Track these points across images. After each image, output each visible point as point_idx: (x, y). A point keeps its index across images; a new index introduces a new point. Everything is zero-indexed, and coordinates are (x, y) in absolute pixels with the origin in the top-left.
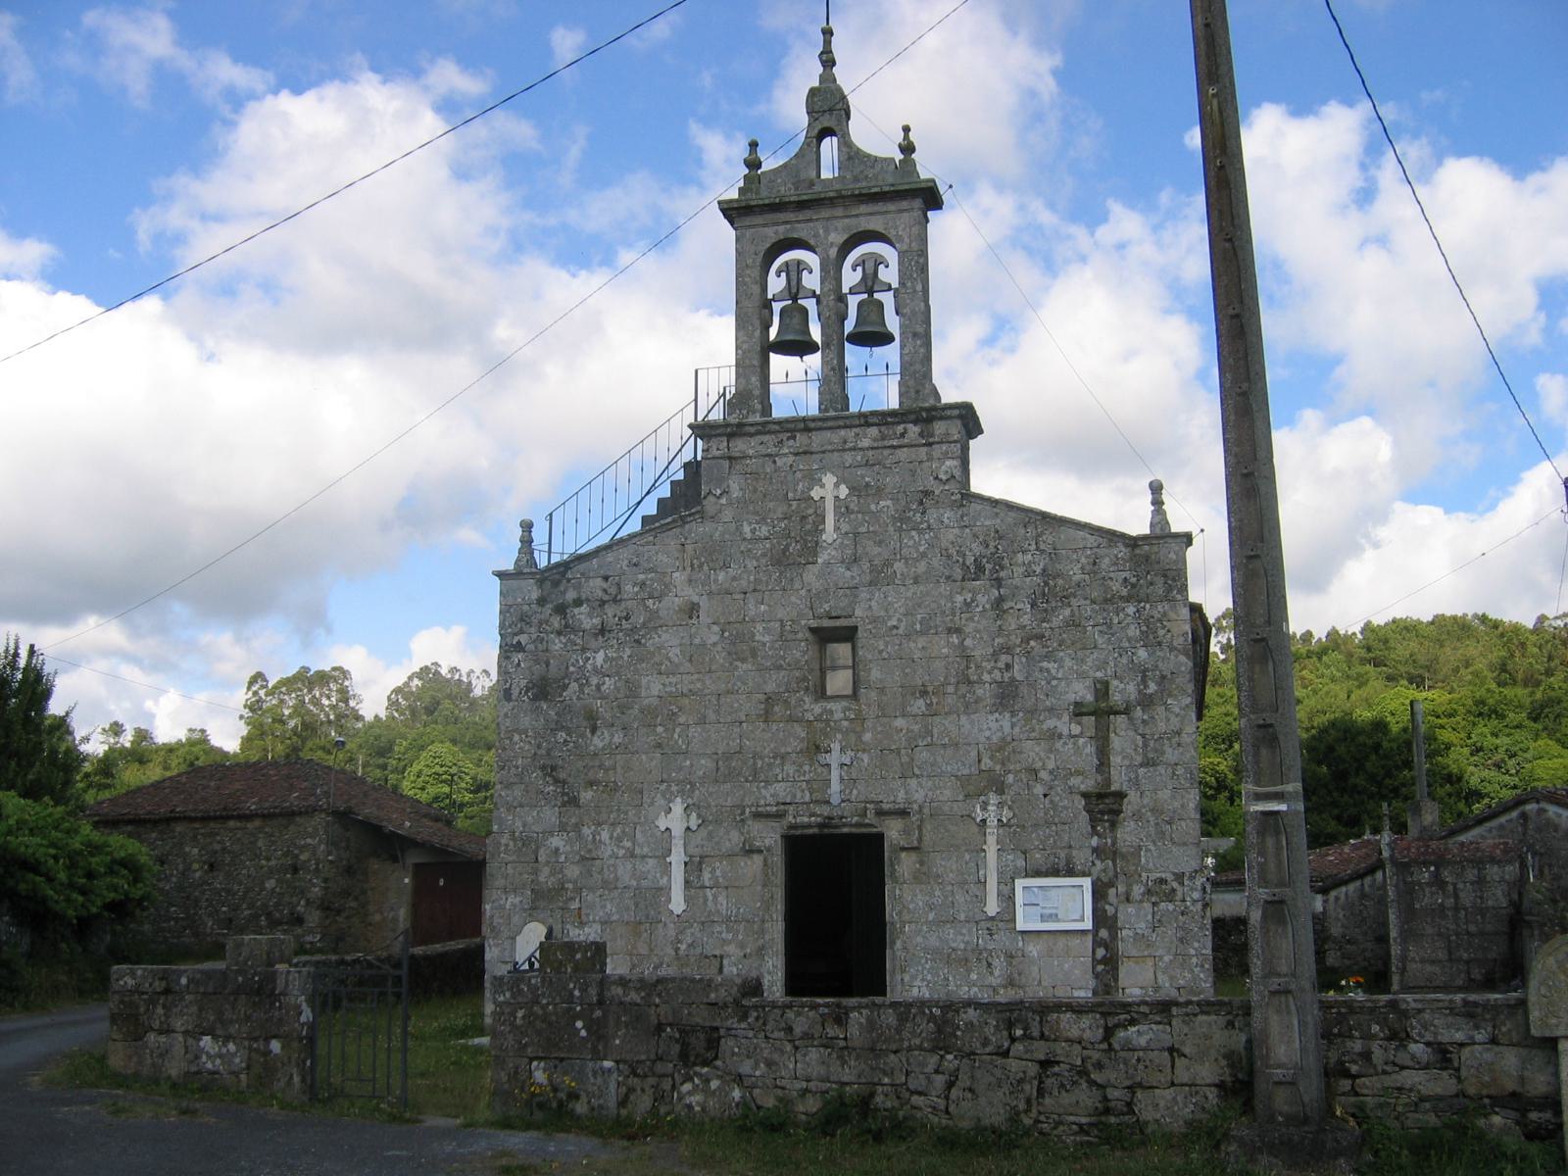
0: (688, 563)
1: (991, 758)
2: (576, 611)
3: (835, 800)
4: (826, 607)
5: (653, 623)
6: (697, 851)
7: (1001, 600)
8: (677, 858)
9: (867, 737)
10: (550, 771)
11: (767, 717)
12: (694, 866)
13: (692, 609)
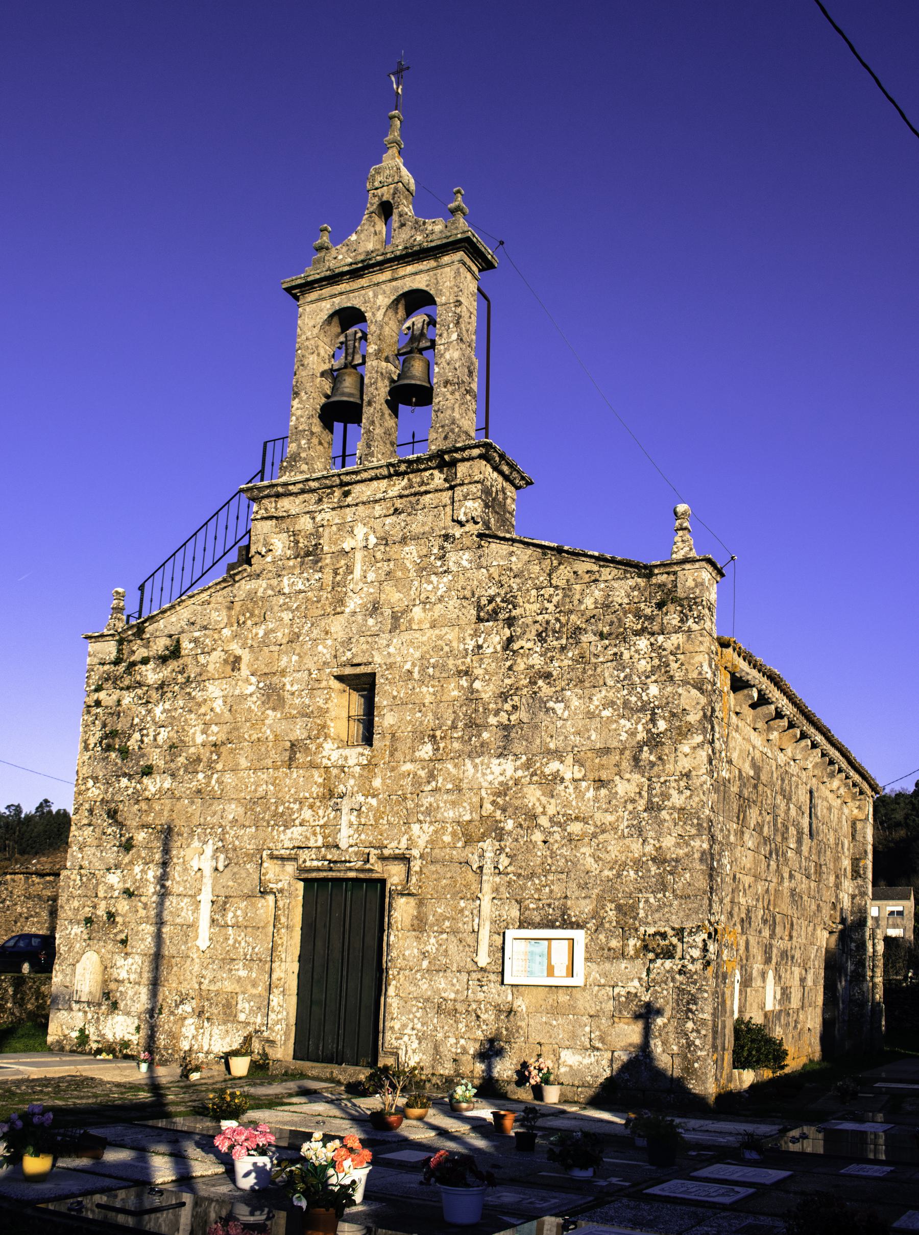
0: (234, 620)
1: (493, 803)
2: (143, 668)
3: (343, 845)
4: (349, 655)
5: (201, 680)
6: (223, 893)
7: (510, 640)
8: (206, 897)
9: (377, 783)
10: (112, 814)
11: (290, 762)
12: (221, 905)
13: (234, 662)
